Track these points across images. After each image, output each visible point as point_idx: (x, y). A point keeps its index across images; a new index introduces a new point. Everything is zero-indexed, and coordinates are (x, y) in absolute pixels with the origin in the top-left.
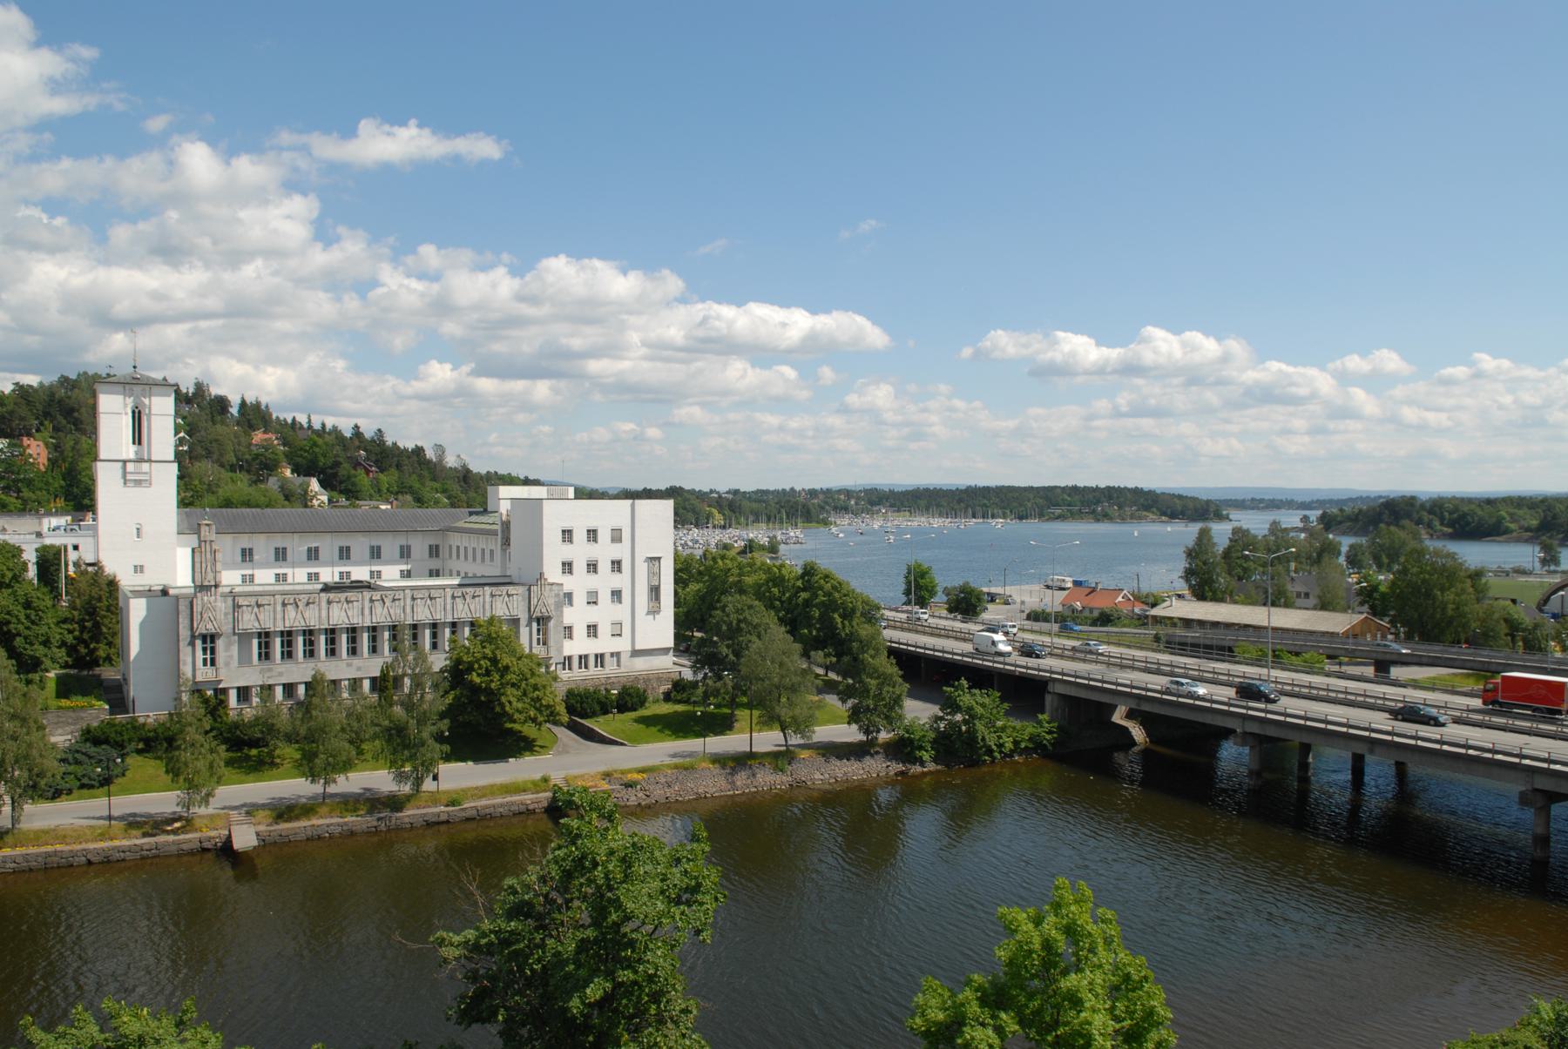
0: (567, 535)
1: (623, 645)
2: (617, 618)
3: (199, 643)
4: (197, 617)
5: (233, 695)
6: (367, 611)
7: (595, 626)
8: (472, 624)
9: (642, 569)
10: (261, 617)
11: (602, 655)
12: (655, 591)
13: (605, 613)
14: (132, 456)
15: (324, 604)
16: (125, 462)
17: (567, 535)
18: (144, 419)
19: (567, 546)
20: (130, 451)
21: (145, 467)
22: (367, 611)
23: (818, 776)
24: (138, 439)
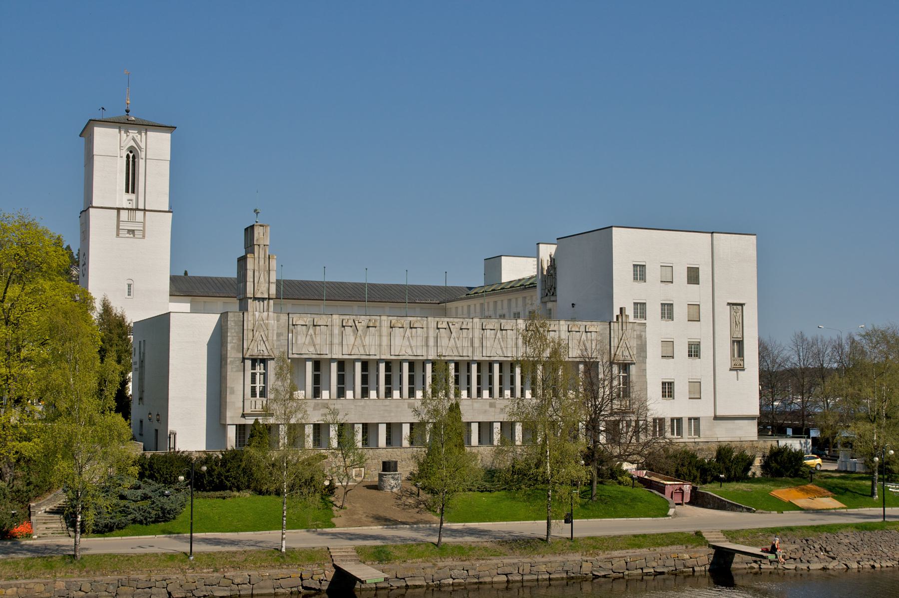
0: (640, 272)
1: (703, 409)
2: (696, 377)
3: (248, 363)
4: (248, 335)
5: (475, 428)
6: (431, 342)
7: (671, 384)
8: (585, 363)
9: (724, 314)
10: (318, 340)
11: (679, 420)
12: (739, 344)
13: (680, 370)
14: (126, 205)
15: (385, 330)
16: (119, 209)
17: (640, 272)
18: (141, 163)
19: (640, 285)
20: (123, 200)
21: (139, 214)
22: (431, 342)
23: (248, 495)
24: (131, 185)
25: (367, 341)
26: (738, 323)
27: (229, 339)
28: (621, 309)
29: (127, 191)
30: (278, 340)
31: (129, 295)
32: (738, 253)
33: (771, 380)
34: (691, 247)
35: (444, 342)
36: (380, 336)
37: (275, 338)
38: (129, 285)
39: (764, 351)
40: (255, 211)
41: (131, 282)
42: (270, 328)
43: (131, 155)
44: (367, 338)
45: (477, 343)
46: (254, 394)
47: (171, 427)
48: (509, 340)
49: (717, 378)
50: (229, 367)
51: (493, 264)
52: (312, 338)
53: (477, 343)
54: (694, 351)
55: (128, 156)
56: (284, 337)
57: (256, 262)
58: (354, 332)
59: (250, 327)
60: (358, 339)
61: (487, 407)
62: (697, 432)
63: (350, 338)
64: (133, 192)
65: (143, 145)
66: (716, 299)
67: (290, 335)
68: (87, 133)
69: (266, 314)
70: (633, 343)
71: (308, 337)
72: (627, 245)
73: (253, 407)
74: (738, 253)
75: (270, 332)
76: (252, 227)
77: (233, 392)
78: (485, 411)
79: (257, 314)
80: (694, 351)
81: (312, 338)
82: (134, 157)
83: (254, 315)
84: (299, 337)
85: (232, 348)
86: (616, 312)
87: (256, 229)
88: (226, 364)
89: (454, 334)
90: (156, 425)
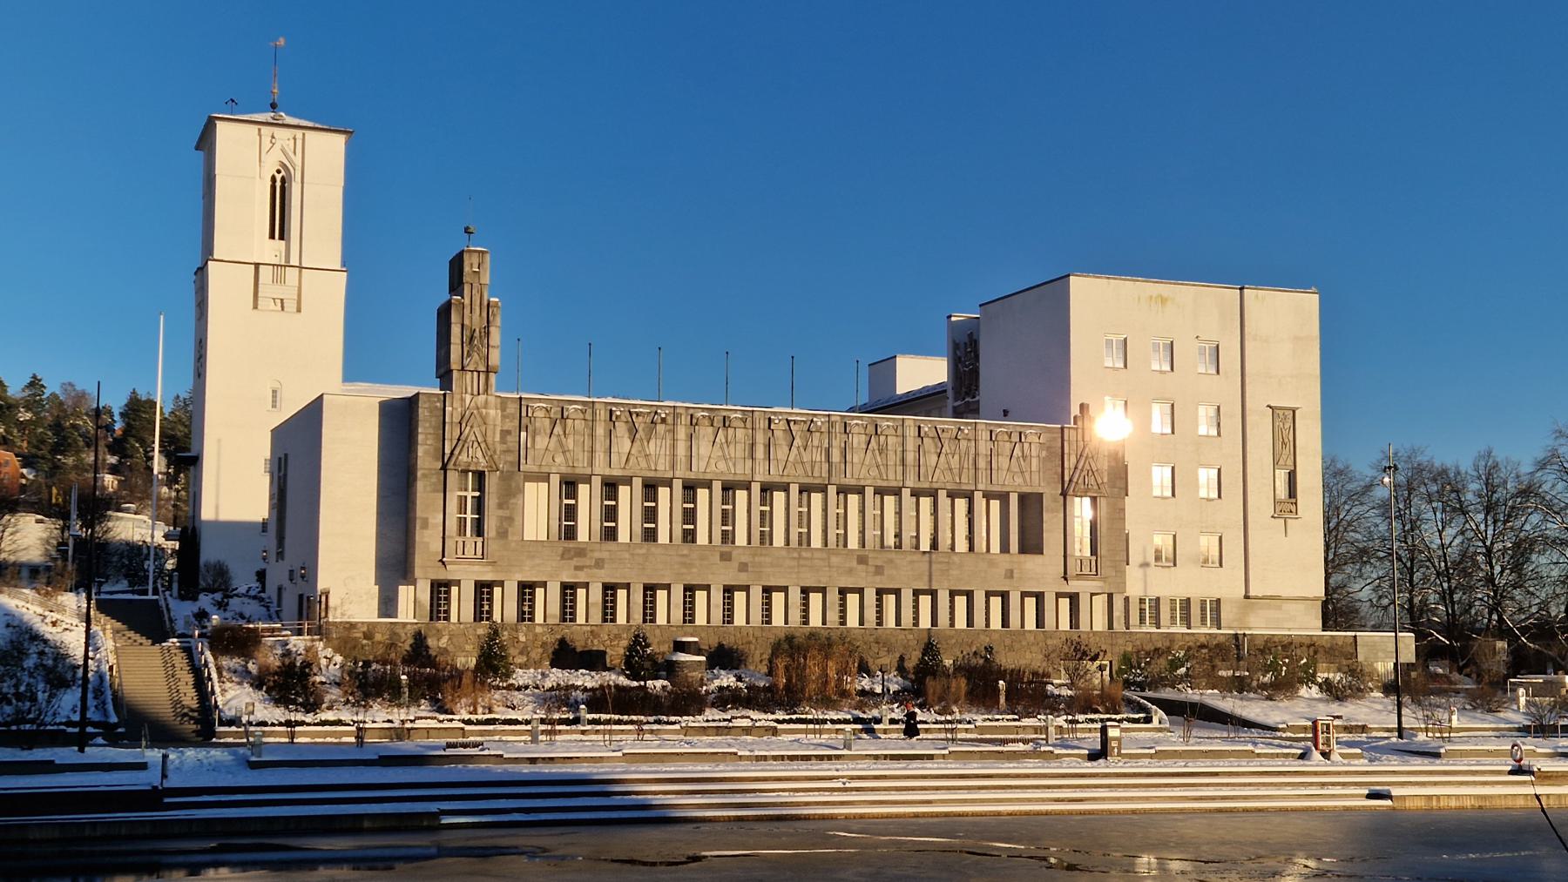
4: (452, 433)
16: (257, 265)
22: (760, 452)
24: (279, 227)
25: (652, 448)
26: (1284, 443)
27: (420, 437)
28: (1082, 406)
29: (272, 236)
30: (503, 441)
31: (274, 406)
32: (1287, 321)
34: (1197, 309)
35: (781, 452)
37: (498, 438)
38: (274, 392)
39: (1334, 475)
40: (467, 230)
41: (277, 385)
43: (279, 177)
44: (652, 443)
45: (836, 456)
47: (321, 585)
48: (891, 455)
49: (1248, 388)
50: (420, 485)
51: (884, 369)
52: (560, 442)
53: (836, 456)
55: (273, 179)
56: (512, 439)
57: (467, 311)
58: (630, 431)
59: (456, 419)
60: (637, 444)
61: (854, 563)
63: (623, 444)
64: (282, 238)
65: (297, 160)
66: (1248, 412)
67: (523, 434)
68: (206, 141)
69: (482, 398)
71: (554, 438)
73: (460, 551)
74: (1287, 321)
75: (490, 428)
77: (425, 525)
79: (468, 398)
81: (560, 442)
82: (283, 179)
83: (463, 400)
84: (538, 438)
85: (426, 452)
86: (1075, 410)
87: (466, 256)
88: (415, 479)
89: (798, 442)
90: (301, 587)
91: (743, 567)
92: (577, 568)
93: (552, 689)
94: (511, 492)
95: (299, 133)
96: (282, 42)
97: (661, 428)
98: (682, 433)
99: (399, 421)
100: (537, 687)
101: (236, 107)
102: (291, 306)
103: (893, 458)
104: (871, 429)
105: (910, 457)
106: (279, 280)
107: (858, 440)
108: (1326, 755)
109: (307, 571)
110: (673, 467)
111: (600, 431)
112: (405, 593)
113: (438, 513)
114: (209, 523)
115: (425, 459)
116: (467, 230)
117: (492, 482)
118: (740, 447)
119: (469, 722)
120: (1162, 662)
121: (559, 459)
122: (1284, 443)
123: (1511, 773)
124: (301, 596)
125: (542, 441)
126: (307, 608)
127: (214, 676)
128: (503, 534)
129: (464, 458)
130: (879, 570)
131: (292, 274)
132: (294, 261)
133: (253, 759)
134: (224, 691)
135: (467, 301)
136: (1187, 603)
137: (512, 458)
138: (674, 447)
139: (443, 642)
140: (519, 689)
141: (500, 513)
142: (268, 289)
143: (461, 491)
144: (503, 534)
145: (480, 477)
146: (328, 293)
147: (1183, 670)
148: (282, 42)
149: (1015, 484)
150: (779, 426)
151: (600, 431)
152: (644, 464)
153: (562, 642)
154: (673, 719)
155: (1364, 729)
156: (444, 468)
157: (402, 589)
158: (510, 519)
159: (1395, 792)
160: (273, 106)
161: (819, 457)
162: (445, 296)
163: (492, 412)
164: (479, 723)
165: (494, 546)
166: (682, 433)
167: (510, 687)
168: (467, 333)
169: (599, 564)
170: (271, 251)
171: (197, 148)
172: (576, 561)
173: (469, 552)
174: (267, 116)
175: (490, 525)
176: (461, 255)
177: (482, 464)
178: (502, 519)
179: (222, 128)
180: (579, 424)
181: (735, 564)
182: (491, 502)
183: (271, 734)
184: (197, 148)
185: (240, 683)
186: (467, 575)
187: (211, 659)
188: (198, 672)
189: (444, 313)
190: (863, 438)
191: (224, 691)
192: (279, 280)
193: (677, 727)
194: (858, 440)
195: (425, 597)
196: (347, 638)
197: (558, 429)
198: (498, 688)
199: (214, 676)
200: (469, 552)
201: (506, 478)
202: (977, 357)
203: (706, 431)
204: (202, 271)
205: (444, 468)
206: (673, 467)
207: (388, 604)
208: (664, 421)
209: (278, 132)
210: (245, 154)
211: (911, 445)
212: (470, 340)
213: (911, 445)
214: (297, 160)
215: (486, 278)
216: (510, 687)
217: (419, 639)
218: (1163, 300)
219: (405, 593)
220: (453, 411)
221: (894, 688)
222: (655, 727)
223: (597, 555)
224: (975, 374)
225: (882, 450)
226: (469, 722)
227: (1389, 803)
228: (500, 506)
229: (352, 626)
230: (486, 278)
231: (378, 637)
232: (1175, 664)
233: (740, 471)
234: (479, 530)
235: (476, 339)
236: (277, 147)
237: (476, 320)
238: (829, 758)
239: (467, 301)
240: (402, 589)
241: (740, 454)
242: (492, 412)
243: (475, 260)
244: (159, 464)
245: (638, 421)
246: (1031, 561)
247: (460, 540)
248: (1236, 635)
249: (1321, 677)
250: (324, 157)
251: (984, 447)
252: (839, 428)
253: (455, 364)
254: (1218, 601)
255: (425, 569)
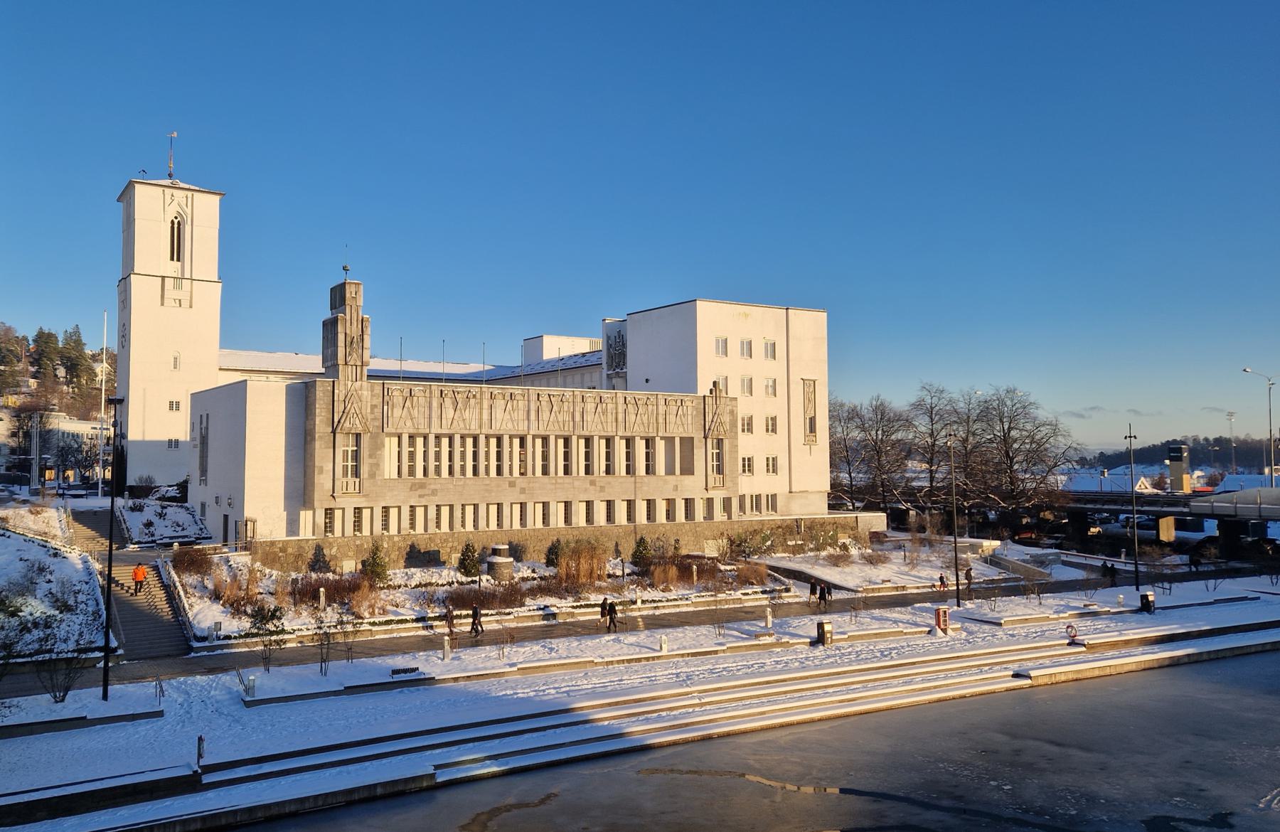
0: (723, 347)
4: (339, 408)
12: (812, 421)
16: (163, 278)
17: (723, 347)
24: (176, 252)
26: (810, 399)
29: (172, 259)
30: (372, 412)
32: (810, 326)
33: (840, 455)
34: (760, 321)
35: (545, 415)
36: (481, 409)
38: (176, 359)
40: (345, 268)
42: (364, 399)
45: (578, 418)
46: (345, 474)
47: (248, 513)
50: (318, 444)
51: (534, 343)
54: (772, 426)
56: (378, 410)
59: (342, 398)
62: (774, 508)
64: (178, 260)
68: (126, 196)
69: (359, 383)
70: (726, 419)
72: (713, 318)
74: (810, 326)
76: (343, 286)
77: (321, 472)
78: (586, 490)
80: (772, 426)
88: (313, 439)
91: (523, 491)
92: (420, 496)
93: (417, 586)
94: (377, 447)
95: (190, 194)
96: (175, 134)
97: (472, 401)
98: (486, 404)
99: (302, 396)
100: (406, 586)
101: (146, 175)
102: (185, 303)
103: (611, 418)
104: (598, 400)
105: (621, 417)
106: (178, 287)
107: (590, 406)
108: (944, 631)
109: (235, 498)
110: (481, 427)
111: (435, 404)
112: (305, 516)
113: (328, 464)
114: (133, 442)
115: (321, 426)
116: (345, 268)
117: (365, 440)
118: (521, 412)
119: (374, 624)
120: (758, 538)
121: (409, 423)
122: (810, 399)
123: (1069, 644)
124: (226, 517)
125: (397, 412)
126: (234, 530)
127: (182, 593)
128: (372, 476)
129: (347, 425)
130: (602, 489)
131: (186, 283)
132: (187, 275)
133: (248, 699)
134: (191, 606)
135: (348, 317)
136: (758, 497)
137: (379, 423)
138: (481, 413)
139: (334, 551)
140: (395, 588)
141: (371, 461)
142: (170, 293)
143: (345, 445)
144: (372, 476)
145: (358, 436)
146: (210, 296)
147: (769, 543)
148: (175, 134)
149: (677, 432)
150: (544, 399)
151: (435, 404)
152: (462, 425)
153: (412, 546)
154: (508, 611)
155: (904, 588)
156: (334, 432)
157: (302, 513)
158: (377, 465)
159: (1033, 673)
160: (170, 176)
161: (568, 418)
162: (328, 314)
163: (365, 393)
164: (381, 624)
165: (366, 484)
166: (486, 404)
167: (389, 587)
168: (349, 339)
169: (434, 493)
170: (172, 268)
171: (118, 200)
172: (420, 492)
173: (351, 489)
174: (167, 182)
175: (365, 470)
176: (343, 286)
177: (359, 429)
178: (371, 465)
179: (139, 189)
180: (422, 400)
181: (518, 489)
182: (365, 452)
183: (237, 645)
184: (118, 200)
185: (200, 598)
186: (350, 503)
187: (176, 579)
188: (169, 590)
189: (330, 327)
190: (594, 405)
191: (191, 606)
192: (178, 287)
193: (511, 617)
194: (590, 406)
195: (321, 519)
196: (271, 554)
197: (408, 403)
198: (382, 589)
199: (182, 593)
200: (351, 489)
201: (374, 437)
202: (624, 345)
203: (500, 403)
204: (124, 283)
205: (334, 432)
206: (481, 427)
207: (293, 526)
208: (474, 396)
209: (176, 192)
210: (153, 206)
211: (621, 409)
212: (350, 343)
213: (621, 408)
214: (189, 211)
215: (361, 302)
216: (389, 587)
217: (319, 549)
218: (746, 315)
219: (305, 516)
220: (340, 392)
221: (627, 571)
222: (498, 618)
223: (433, 487)
224: (623, 355)
225: (605, 412)
226: (374, 624)
227: (1029, 682)
228: (370, 456)
229: (273, 543)
230: (361, 302)
231: (290, 550)
232: (765, 539)
233: (522, 429)
234: (356, 473)
235: (357, 343)
236: (175, 202)
237: (354, 331)
238: (653, 658)
239: (348, 317)
240: (302, 513)
241: (521, 417)
242: (365, 393)
243: (353, 289)
244: (61, 372)
245: (458, 397)
246: (688, 479)
247: (345, 480)
248: (796, 520)
249: (841, 541)
250: (205, 211)
251: (662, 408)
252: (579, 399)
253: (341, 361)
254: (774, 496)
255: (321, 498)
